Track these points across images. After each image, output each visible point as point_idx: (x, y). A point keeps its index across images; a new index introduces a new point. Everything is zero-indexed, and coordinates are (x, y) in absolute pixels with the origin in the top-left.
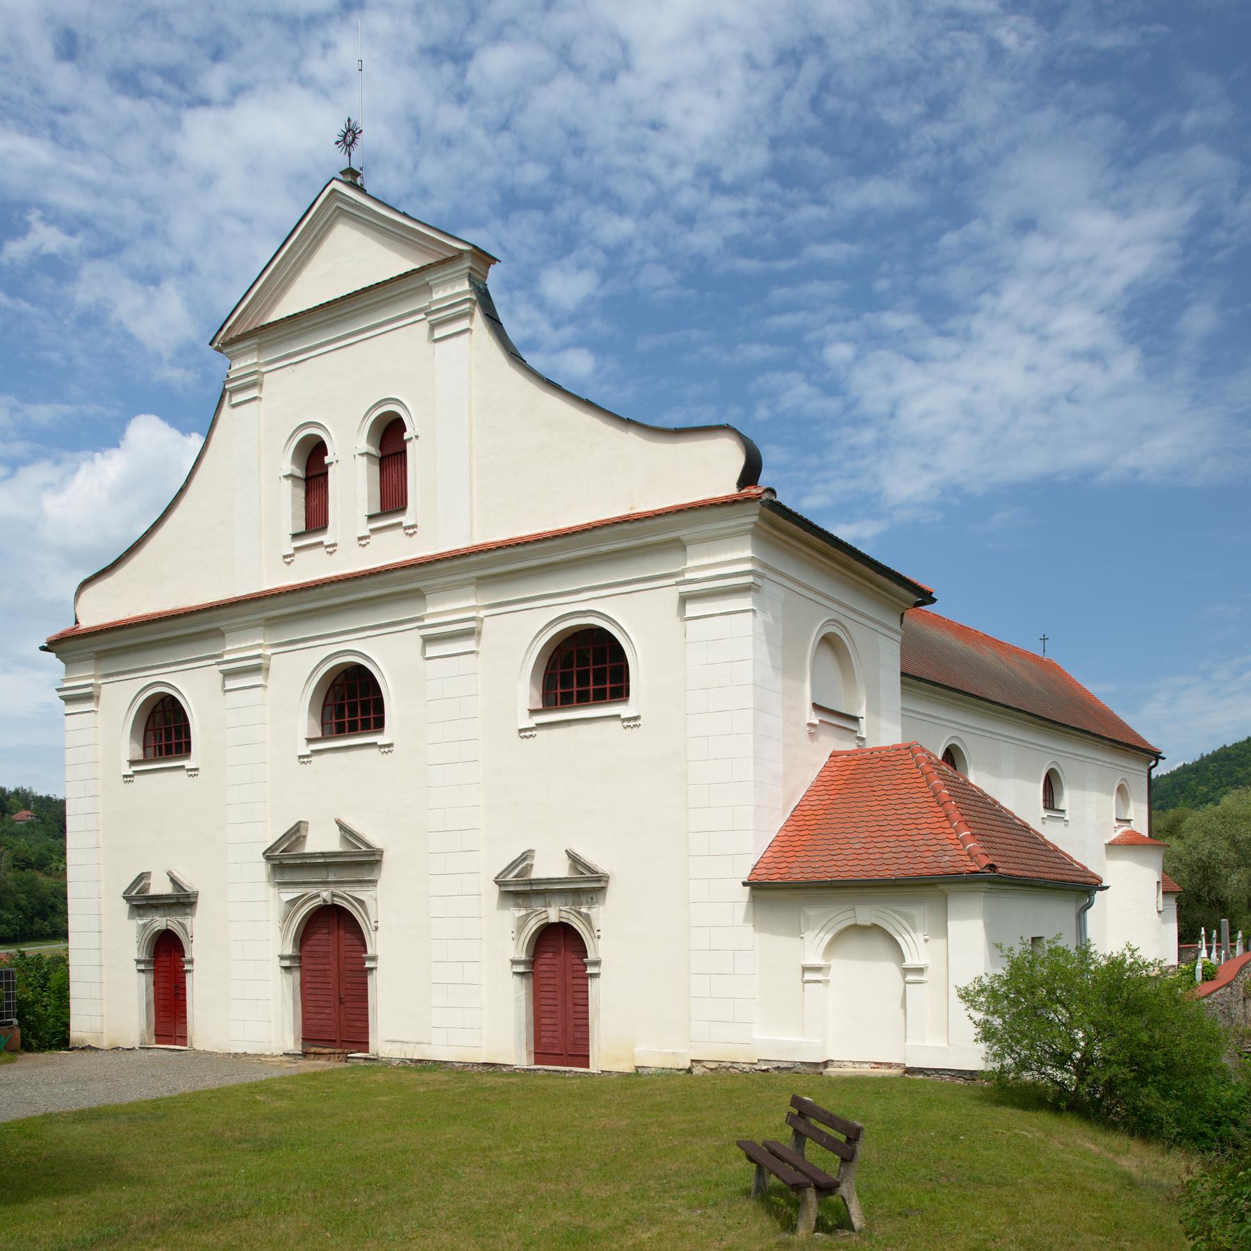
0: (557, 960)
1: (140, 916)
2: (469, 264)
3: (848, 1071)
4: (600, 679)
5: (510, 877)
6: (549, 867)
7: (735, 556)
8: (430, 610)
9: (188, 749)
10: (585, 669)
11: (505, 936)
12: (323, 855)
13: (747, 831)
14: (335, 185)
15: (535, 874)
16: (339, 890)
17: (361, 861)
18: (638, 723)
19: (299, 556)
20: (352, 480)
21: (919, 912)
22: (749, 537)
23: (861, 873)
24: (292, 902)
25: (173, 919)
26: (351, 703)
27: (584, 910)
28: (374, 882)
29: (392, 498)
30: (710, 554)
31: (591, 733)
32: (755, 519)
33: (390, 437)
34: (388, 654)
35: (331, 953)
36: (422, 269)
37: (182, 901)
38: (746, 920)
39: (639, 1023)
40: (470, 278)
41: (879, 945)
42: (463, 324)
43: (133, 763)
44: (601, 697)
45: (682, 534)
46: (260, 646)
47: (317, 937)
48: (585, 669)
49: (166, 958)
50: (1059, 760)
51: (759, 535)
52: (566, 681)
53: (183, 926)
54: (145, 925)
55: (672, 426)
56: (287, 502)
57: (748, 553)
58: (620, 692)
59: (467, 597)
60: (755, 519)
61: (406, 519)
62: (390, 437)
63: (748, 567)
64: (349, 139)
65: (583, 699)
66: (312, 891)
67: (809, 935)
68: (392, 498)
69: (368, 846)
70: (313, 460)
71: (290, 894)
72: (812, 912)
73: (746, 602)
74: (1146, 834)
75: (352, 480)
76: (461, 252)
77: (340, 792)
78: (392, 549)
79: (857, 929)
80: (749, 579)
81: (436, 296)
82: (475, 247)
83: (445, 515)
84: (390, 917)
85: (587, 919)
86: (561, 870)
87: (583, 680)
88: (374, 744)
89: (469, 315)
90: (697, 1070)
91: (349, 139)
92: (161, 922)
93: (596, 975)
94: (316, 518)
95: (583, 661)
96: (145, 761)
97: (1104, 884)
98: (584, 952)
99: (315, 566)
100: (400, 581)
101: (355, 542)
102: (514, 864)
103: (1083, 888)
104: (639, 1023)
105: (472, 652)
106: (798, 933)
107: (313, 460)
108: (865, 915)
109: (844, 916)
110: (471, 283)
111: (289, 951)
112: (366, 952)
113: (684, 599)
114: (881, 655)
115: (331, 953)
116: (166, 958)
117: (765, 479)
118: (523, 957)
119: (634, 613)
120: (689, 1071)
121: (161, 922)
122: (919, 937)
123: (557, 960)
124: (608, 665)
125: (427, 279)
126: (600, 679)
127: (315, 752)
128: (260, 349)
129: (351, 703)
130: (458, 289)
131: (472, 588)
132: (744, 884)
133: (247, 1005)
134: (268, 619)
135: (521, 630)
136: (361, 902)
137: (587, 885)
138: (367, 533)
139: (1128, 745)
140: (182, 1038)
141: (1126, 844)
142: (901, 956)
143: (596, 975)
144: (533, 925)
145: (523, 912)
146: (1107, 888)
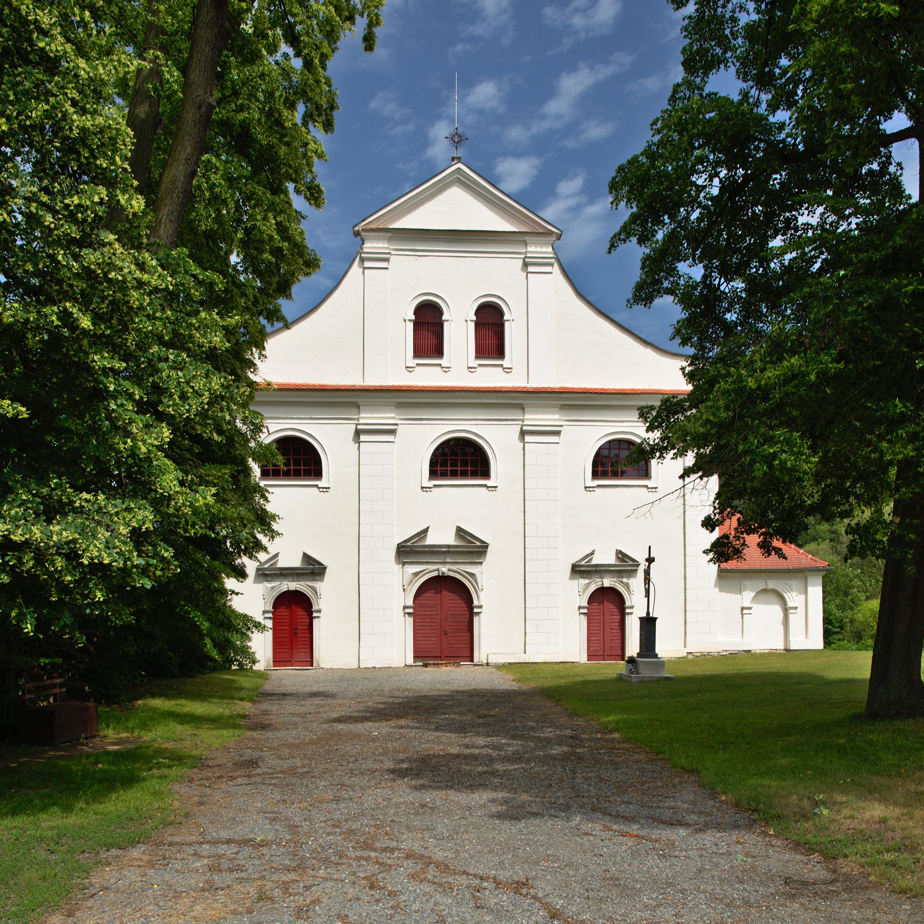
1: (268, 581)
5: (583, 563)
6: (605, 557)
10: (460, 460)
11: (578, 593)
12: (448, 546)
16: (454, 567)
17: (472, 548)
19: (418, 368)
20: (459, 333)
21: (794, 583)
24: (416, 574)
25: (302, 583)
27: (625, 580)
28: (481, 563)
30: (548, 413)
34: (495, 435)
36: (520, 232)
38: (715, 586)
41: (772, 597)
42: (548, 269)
44: (475, 474)
45: (359, 400)
46: (393, 418)
47: (425, 595)
53: (314, 590)
54: (273, 587)
59: (554, 414)
61: (443, 362)
66: (437, 567)
67: (745, 593)
71: (412, 569)
72: (747, 583)
75: (459, 333)
76: (552, 232)
77: (452, 509)
78: (489, 377)
79: (765, 591)
81: (529, 249)
85: (627, 586)
86: (611, 559)
88: (485, 486)
89: (552, 265)
90: (690, 657)
93: (631, 613)
98: (311, 605)
100: (512, 398)
102: (587, 556)
106: (740, 592)
108: (772, 584)
109: (761, 585)
110: (553, 249)
111: (410, 603)
113: (358, 433)
118: (271, 609)
120: (686, 657)
122: (794, 594)
123: (606, 605)
128: (389, 240)
130: (544, 249)
131: (557, 409)
134: (399, 403)
136: (472, 575)
143: (631, 613)
145: (587, 581)
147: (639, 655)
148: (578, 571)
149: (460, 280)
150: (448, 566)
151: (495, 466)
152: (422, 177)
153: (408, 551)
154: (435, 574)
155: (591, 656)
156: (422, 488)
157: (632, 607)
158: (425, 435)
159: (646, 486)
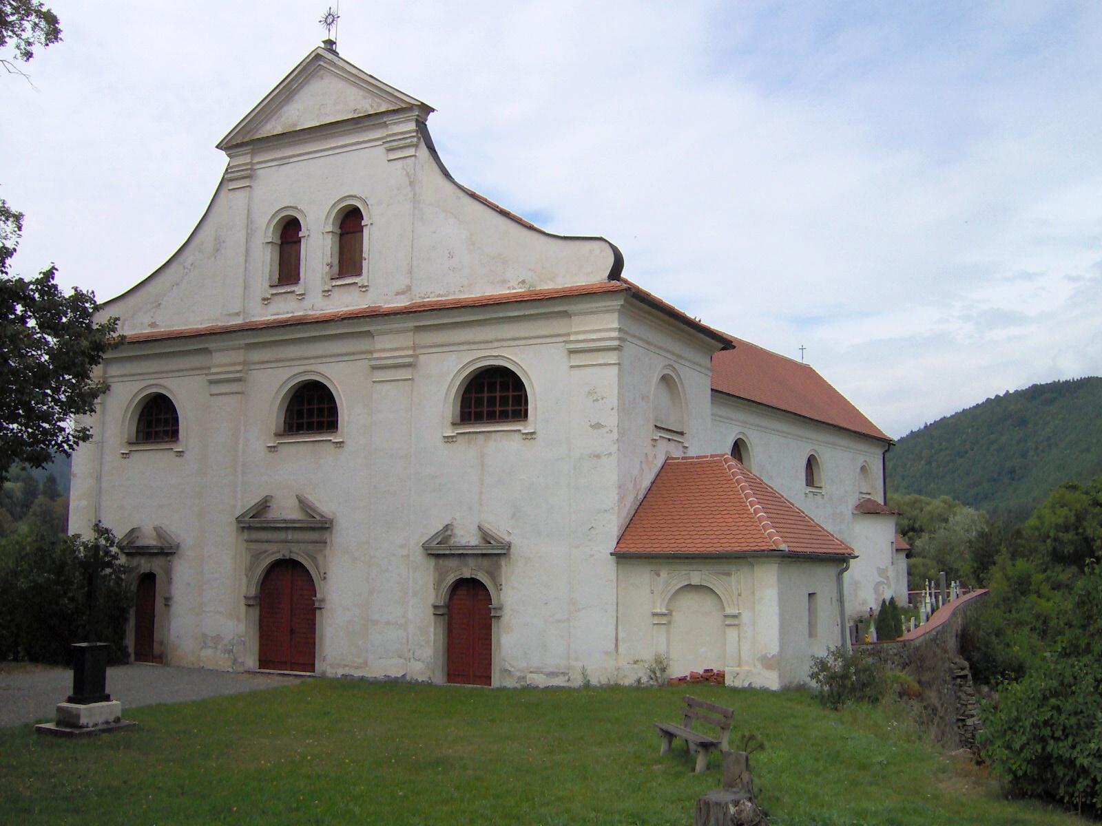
2: (417, 113)
4: (504, 401)
7: (604, 324)
8: (379, 346)
10: (494, 397)
12: (285, 521)
13: (605, 510)
14: (320, 51)
18: (534, 436)
20: (318, 248)
22: (616, 315)
23: (694, 549)
26: (311, 410)
31: (500, 443)
32: (622, 302)
40: (417, 121)
42: (411, 152)
43: (130, 443)
44: (504, 417)
48: (494, 397)
50: (816, 448)
51: (622, 312)
52: (479, 402)
55: (562, 235)
56: (265, 260)
57: (616, 325)
58: (520, 412)
60: (622, 302)
62: (350, 222)
63: (615, 334)
64: (329, 20)
65: (492, 417)
69: (322, 516)
73: (612, 358)
74: (883, 504)
75: (318, 248)
78: (346, 301)
80: (616, 343)
82: (422, 103)
87: (492, 402)
91: (329, 20)
95: (492, 387)
97: (856, 554)
99: (286, 308)
101: (318, 294)
103: (840, 560)
105: (410, 379)
107: (289, 231)
108: (696, 578)
112: (315, 596)
114: (697, 382)
119: (538, 363)
124: (511, 394)
125: (385, 120)
126: (504, 401)
132: (611, 554)
135: (448, 367)
138: (330, 288)
139: (864, 435)
141: (867, 510)
142: (724, 609)
144: (451, 579)
146: (857, 557)
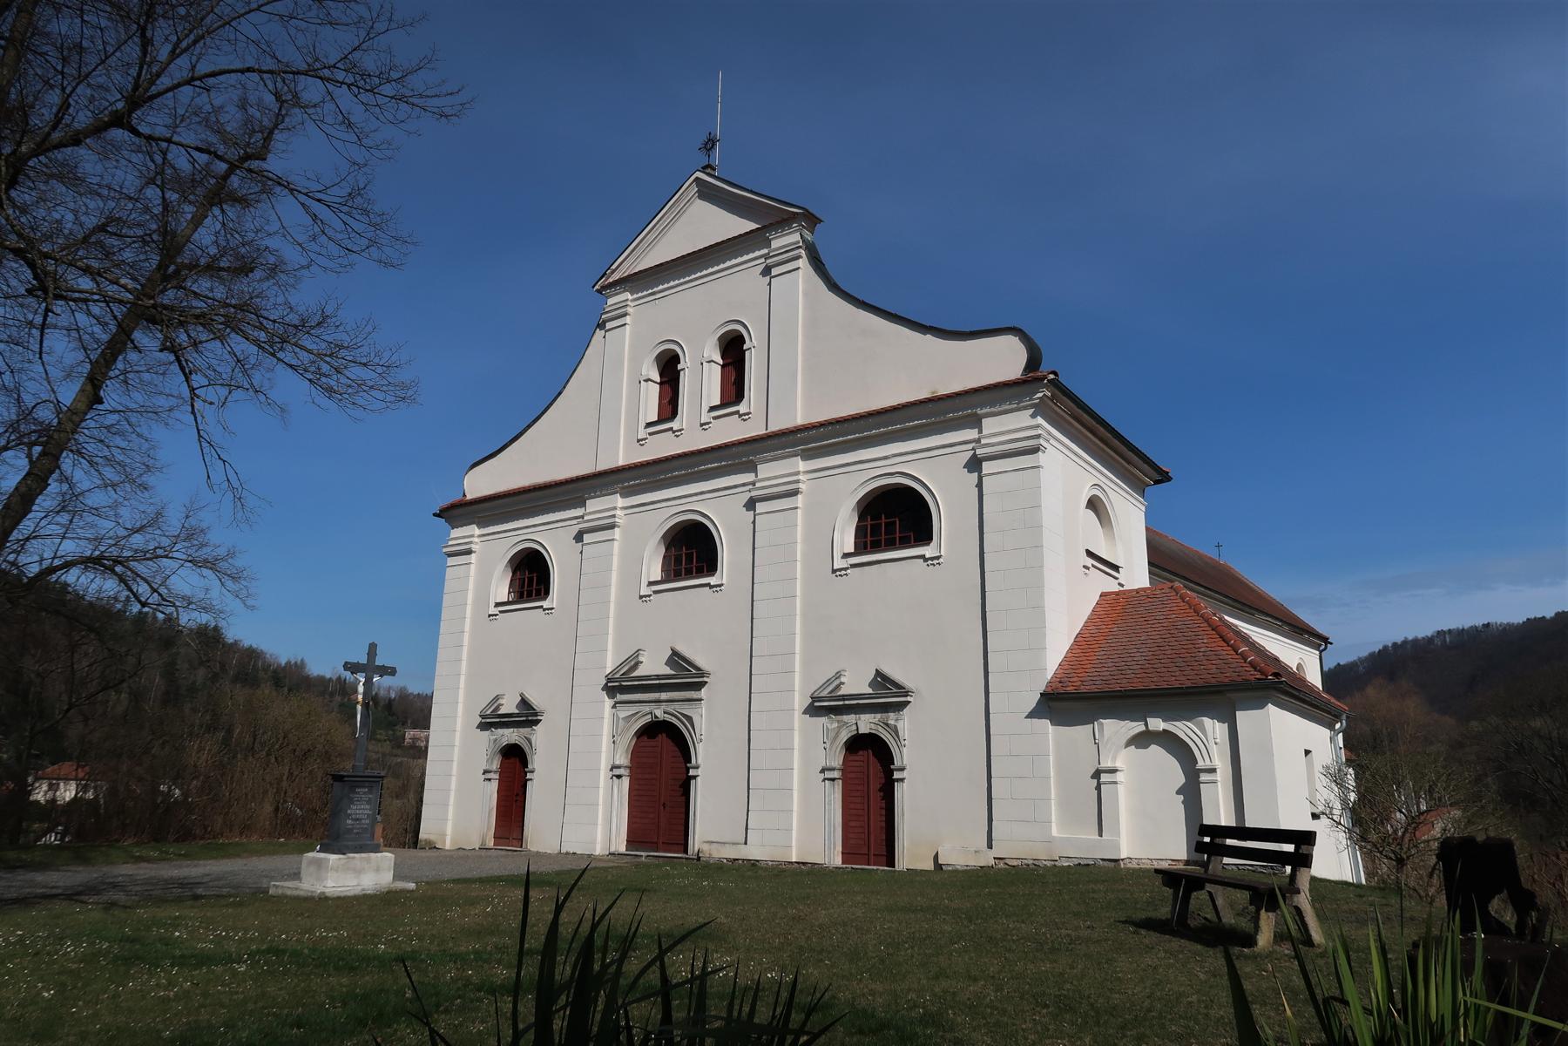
0: (869, 772)
3: (1134, 865)
5: (825, 693)
6: (857, 683)
9: (547, 593)
10: (895, 519)
12: (658, 677)
15: (843, 691)
16: (671, 708)
17: (685, 676)
20: (703, 379)
26: (691, 551)
29: (734, 390)
31: (900, 570)
33: (733, 349)
35: (661, 767)
37: (527, 716)
39: (937, 826)
49: (514, 763)
62: (733, 349)
66: (646, 708)
68: (734, 390)
69: (698, 669)
70: (669, 366)
71: (624, 712)
78: (729, 430)
83: (788, 394)
84: (711, 729)
92: (510, 736)
93: (902, 780)
94: (669, 408)
96: (856, 553)
99: (664, 446)
104: (937, 826)
107: (669, 366)
115: (661, 767)
116: (514, 763)
117: (1044, 368)
121: (510, 736)
123: (869, 772)
127: (656, 592)
129: (691, 551)
133: (583, 815)
137: (889, 694)
140: (520, 839)
143: (902, 780)
144: (845, 736)
147: (70, 759)
148: (816, 708)
149: (691, 317)
150: (664, 706)
151: (725, 556)
152: (648, 210)
153: (620, 686)
154: (648, 719)
155: (847, 855)
156: (834, 571)
157: (902, 769)
158: (833, 493)
159: (923, 557)
